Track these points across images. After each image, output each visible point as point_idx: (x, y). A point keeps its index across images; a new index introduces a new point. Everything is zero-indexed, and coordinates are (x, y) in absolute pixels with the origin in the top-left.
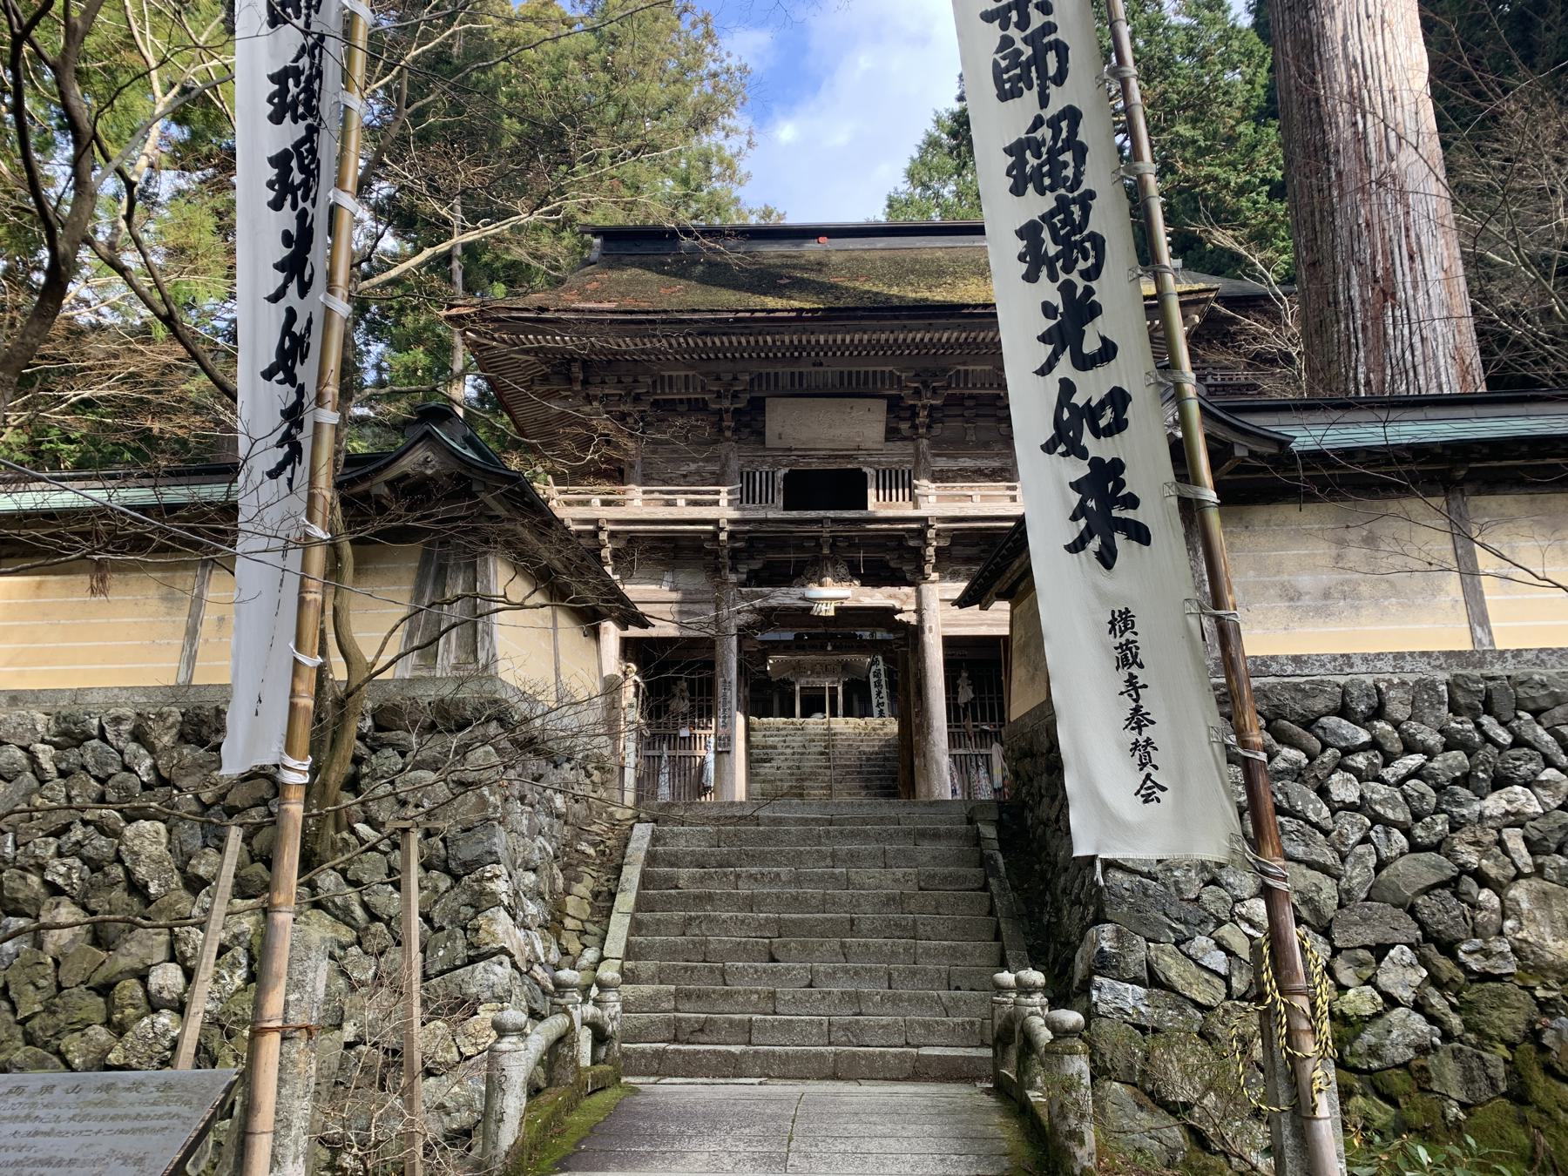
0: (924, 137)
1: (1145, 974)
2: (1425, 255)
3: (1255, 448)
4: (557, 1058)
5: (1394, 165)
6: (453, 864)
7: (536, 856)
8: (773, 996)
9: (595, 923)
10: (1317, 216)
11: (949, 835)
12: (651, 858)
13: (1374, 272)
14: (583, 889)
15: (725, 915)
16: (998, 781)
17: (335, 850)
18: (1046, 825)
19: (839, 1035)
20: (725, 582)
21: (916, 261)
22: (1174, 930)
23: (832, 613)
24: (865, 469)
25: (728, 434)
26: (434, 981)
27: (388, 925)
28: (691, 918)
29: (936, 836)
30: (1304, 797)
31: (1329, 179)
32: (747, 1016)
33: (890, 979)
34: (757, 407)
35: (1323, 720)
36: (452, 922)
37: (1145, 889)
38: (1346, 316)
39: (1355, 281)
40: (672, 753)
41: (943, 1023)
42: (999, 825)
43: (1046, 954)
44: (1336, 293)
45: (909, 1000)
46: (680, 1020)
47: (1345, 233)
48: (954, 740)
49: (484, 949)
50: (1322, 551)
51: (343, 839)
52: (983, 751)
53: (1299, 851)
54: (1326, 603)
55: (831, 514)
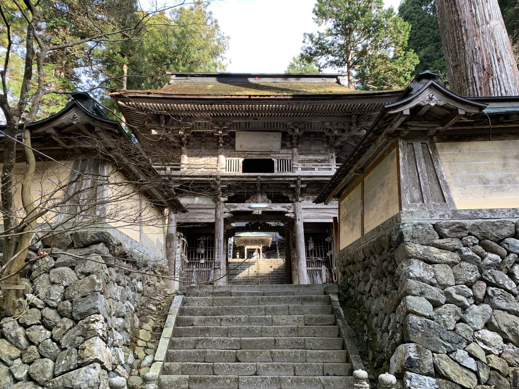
0: (289, 64)
1: (433, 371)
2: (504, 59)
3: (468, 111)
5: (488, 25)
6: (74, 315)
7: (124, 310)
9: (152, 343)
10: (457, 47)
11: (317, 300)
12: (182, 311)
13: (483, 67)
14: (148, 326)
15: (215, 339)
16: (324, 280)
17: (15, 307)
18: (362, 294)
21: (292, 85)
22: (446, 346)
24: (273, 159)
25: (221, 145)
26: (57, 378)
27: (38, 347)
28: (198, 340)
29: (311, 300)
30: (502, 277)
31: (462, 32)
34: (233, 135)
35: (507, 240)
36: (71, 345)
37: (429, 325)
38: (472, 84)
39: (475, 70)
40: (197, 269)
42: (339, 295)
43: (367, 356)
44: (467, 76)
45: (305, 381)
50: (497, 162)
51: (19, 302)
52: (319, 268)
53: (503, 304)
54: (501, 185)
55: (261, 174)
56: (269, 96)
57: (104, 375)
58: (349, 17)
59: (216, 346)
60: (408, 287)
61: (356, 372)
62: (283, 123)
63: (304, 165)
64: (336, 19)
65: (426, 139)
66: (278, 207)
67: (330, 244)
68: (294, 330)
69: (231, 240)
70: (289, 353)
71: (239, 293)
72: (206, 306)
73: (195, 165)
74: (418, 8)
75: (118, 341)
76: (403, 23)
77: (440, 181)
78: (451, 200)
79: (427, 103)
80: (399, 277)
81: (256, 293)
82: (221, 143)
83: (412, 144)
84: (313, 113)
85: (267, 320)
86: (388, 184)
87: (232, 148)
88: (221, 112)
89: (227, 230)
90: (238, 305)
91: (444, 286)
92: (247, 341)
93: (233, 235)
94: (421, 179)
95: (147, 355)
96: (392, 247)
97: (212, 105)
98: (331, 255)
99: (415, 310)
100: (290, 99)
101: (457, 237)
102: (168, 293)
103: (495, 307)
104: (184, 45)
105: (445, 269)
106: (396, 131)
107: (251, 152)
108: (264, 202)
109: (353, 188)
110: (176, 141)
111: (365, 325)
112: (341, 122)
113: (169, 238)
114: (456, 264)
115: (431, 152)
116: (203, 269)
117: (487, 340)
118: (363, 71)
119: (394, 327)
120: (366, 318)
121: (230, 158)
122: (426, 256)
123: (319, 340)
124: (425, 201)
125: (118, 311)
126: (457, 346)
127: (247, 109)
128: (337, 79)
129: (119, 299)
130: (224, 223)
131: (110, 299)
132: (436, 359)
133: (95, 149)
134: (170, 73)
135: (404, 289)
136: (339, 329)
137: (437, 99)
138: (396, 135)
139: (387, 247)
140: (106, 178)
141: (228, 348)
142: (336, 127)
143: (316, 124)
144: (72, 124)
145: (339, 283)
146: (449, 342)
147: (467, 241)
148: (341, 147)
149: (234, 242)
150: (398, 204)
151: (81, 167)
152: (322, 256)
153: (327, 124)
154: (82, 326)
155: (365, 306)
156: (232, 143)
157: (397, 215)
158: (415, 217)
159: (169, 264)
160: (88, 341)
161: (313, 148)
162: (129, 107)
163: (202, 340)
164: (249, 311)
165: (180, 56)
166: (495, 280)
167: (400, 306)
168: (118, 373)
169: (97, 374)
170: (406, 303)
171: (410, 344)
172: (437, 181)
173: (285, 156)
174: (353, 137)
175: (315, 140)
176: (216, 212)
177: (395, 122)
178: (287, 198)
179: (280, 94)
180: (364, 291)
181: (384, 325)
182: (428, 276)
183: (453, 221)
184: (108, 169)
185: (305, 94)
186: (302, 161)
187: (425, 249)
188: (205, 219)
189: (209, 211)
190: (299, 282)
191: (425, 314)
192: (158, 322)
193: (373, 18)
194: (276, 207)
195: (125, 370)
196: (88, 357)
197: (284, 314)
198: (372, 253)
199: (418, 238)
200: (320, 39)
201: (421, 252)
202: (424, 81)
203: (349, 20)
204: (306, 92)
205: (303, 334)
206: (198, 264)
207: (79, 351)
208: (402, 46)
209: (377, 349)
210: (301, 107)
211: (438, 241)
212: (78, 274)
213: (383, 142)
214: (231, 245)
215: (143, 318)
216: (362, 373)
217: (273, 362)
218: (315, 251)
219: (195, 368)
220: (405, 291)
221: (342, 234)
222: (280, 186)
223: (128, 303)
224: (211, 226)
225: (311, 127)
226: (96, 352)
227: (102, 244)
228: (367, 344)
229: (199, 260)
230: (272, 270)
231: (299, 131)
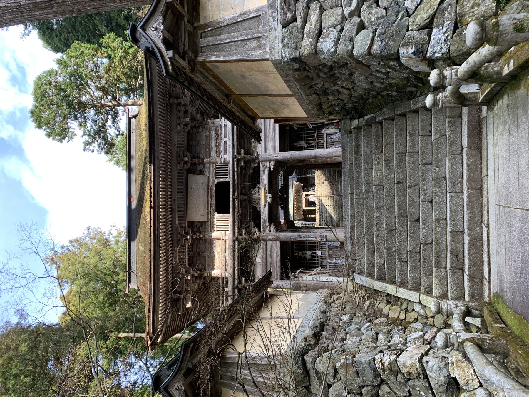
0: (115, 165)
1: (426, 31)
4: (491, 349)
6: (376, 383)
7: (370, 333)
8: (437, 220)
9: (402, 304)
11: (357, 141)
12: (370, 275)
18: (351, 96)
19: (457, 188)
20: (258, 237)
21: (139, 164)
22: (402, 18)
23: (270, 195)
24: (216, 183)
25: (202, 236)
28: (399, 259)
29: (357, 147)
32: (449, 234)
33: (427, 164)
34: (191, 224)
37: (381, 34)
41: (450, 136)
42: (352, 119)
43: (411, 92)
45: (437, 154)
46: (452, 267)
48: (321, 147)
49: (420, 371)
52: (325, 136)
55: (231, 195)
56: (151, 187)
57: (434, 353)
58: (67, 105)
59: (404, 241)
60: (345, 54)
61: (428, 106)
62: (178, 173)
63: (222, 151)
64: (68, 118)
65: (197, 33)
66: (264, 178)
67: (300, 125)
68: (387, 164)
69: (298, 223)
70: (410, 169)
71: (351, 218)
72: (365, 251)
73: (222, 263)
74: (56, 32)
75: (401, 339)
76: (72, 49)
77: (239, 20)
78: (258, 10)
79: (161, 33)
80: (335, 62)
81: (351, 201)
82: (199, 236)
83: (202, 47)
84: (168, 142)
85: (378, 191)
86: (242, 71)
87: (205, 225)
88: (167, 236)
89: (288, 228)
90: (363, 219)
91: (344, 18)
92: (399, 210)
93: (293, 222)
94: (237, 39)
95: (413, 310)
96: (305, 68)
97: (160, 247)
98: (312, 124)
99: (367, 47)
100: (154, 166)
101: (295, 4)
102: (352, 289)
104: (97, 274)
105: (327, 17)
107: (209, 205)
108: (259, 192)
109: (246, 105)
110: (198, 282)
111: (382, 93)
112: (177, 114)
113: (297, 288)
114: (321, 6)
115: (210, 29)
116: (327, 254)
118: (123, 90)
119: (384, 66)
120: (374, 93)
121: (215, 226)
122: (314, 35)
123: (397, 139)
124: (260, 35)
125: (371, 340)
126: (401, 6)
127: (164, 210)
128: (132, 118)
129: (360, 338)
130: (280, 232)
131: (360, 347)
132: (415, 27)
133: (211, 368)
134: (127, 289)
135: (347, 57)
136: (386, 119)
137: (157, 23)
138: (193, 63)
139: (306, 73)
140: (240, 355)
141: (406, 229)
142: (182, 119)
143: (179, 139)
144: (185, 390)
145: (340, 118)
146: (398, 15)
148: (202, 114)
149: (299, 220)
150: (263, 62)
151: (228, 380)
152: (312, 133)
153: (179, 128)
154: (387, 376)
155: (363, 93)
156: (199, 225)
157: (273, 63)
158: (275, 46)
159: (323, 288)
160: (401, 369)
161: (204, 142)
162: (163, 331)
163: (398, 255)
164: (369, 209)
165: (109, 279)
167: (363, 62)
168: (432, 338)
169: (434, 359)
170: (360, 56)
171: (400, 52)
172: (239, 23)
173: (212, 171)
174: (192, 101)
175: (195, 140)
176: (270, 240)
177: (180, 65)
178: (254, 168)
179: (149, 177)
180: (349, 94)
181: (382, 76)
182: (333, 34)
183: (279, 9)
184: (229, 353)
185: (148, 151)
187: (307, 36)
188: (277, 252)
189: (269, 248)
190: (339, 156)
191: (371, 38)
192: (381, 299)
193: (68, 80)
194: (264, 180)
195: (429, 331)
196: (417, 369)
197: (372, 173)
198: (311, 87)
199: (297, 43)
200: (89, 135)
201: (310, 40)
202: (138, 35)
203: (70, 105)
204: (146, 150)
205: (391, 155)
206: (322, 257)
207: (411, 378)
208: (96, 51)
209: (405, 82)
210: (161, 155)
211: (299, 23)
212: (336, 380)
213: (200, 76)
214: (302, 224)
215: (378, 314)
216: (429, 100)
217: (419, 185)
218: (307, 140)
219: (426, 262)
220: (349, 56)
221: (292, 115)
222: (243, 176)
223: (363, 330)
224: (285, 246)
225: (183, 144)
226: (412, 361)
227: (305, 357)
228: (400, 92)
229: (318, 257)
230: (326, 182)
231: (186, 156)
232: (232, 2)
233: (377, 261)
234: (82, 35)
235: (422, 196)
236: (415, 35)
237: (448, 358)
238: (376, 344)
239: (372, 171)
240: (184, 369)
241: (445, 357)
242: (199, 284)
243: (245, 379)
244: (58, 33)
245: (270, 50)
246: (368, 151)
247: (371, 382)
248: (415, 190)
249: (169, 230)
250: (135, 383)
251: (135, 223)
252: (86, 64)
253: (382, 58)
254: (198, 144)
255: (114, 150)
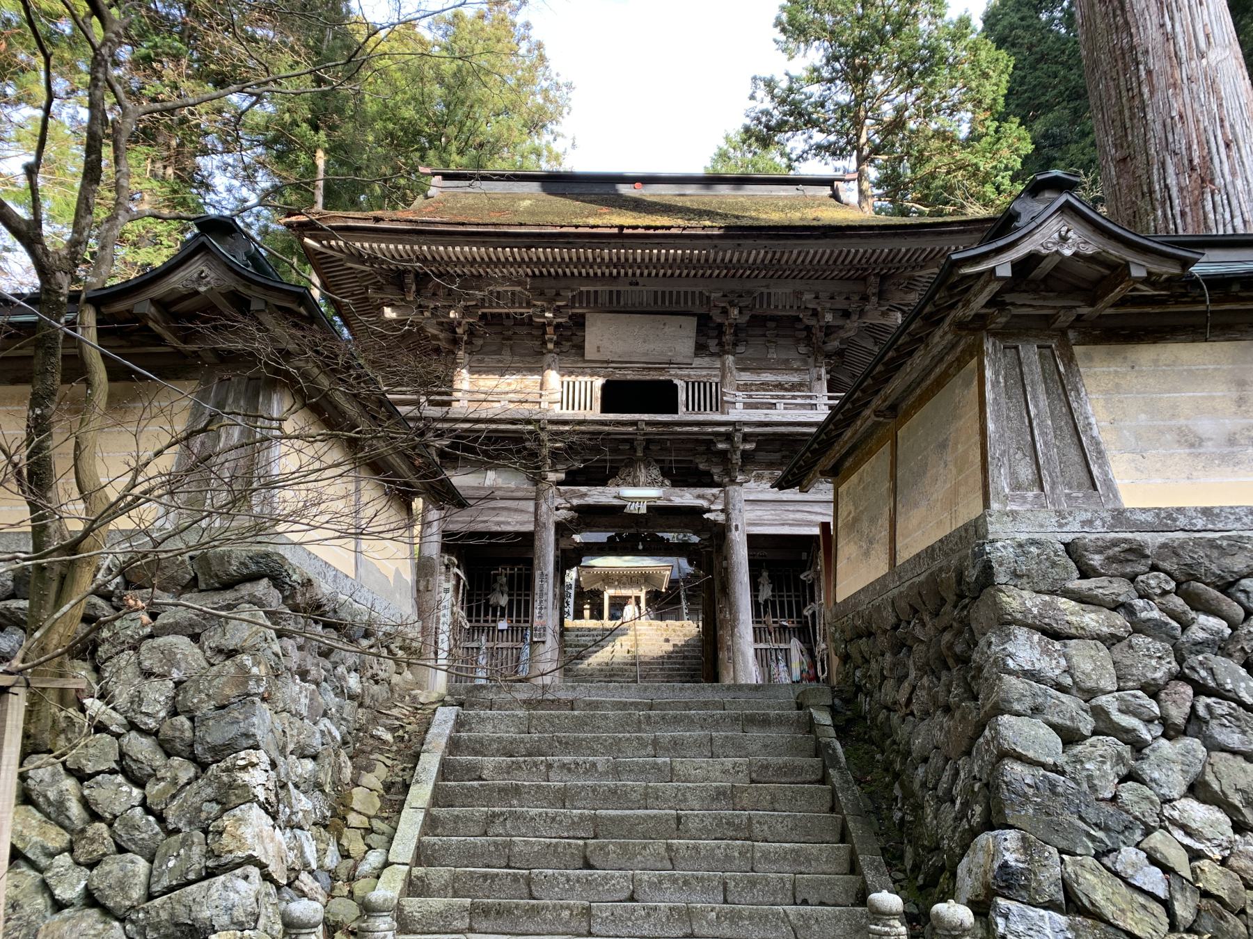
0: (716, 151)
2: (1241, 144)
5: (1204, 61)
6: (199, 750)
7: (317, 741)
9: (384, 819)
11: (780, 721)
12: (454, 745)
13: (1191, 161)
14: (373, 780)
15: (534, 811)
16: (796, 674)
18: (889, 710)
21: (722, 203)
22: (1093, 839)
23: (644, 511)
24: (676, 381)
25: (550, 346)
26: (157, 902)
27: (110, 825)
28: (494, 815)
29: (765, 722)
30: (1232, 674)
31: (1138, 78)
33: (725, 890)
34: (579, 323)
35: (1243, 581)
36: (190, 823)
37: (1053, 786)
38: (1163, 204)
39: (1171, 170)
40: (491, 644)
42: (833, 710)
43: (901, 858)
44: (1150, 184)
45: (751, 918)
47: (1158, 127)
48: (758, 635)
52: (783, 646)
55: (646, 417)
56: (669, 228)
57: (268, 894)
58: (862, 39)
59: (535, 829)
60: (1002, 694)
62: (701, 293)
63: (750, 397)
65: (1051, 337)
66: (686, 497)
67: (812, 586)
68: (724, 793)
69: (571, 575)
71: (592, 702)
73: (484, 392)
74: (1031, 17)
75: (301, 814)
76: (994, 54)
77: (1084, 439)
78: (1109, 484)
79: (1055, 249)
80: (980, 669)
81: (632, 704)
83: (1016, 348)
84: (775, 270)
85: (659, 770)
86: (956, 444)
87: (577, 354)
88: (552, 266)
89: (563, 551)
90: (591, 732)
91: (1090, 694)
93: (578, 563)
94: (1036, 432)
95: (370, 848)
97: (528, 248)
98: (813, 614)
99: (1019, 750)
101: (1123, 575)
102: (422, 700)
103: (1213, 746)
104: (463, 103)
105: (1093, 653)
106: (978, 317)
107: (623, 364)
108: (652, 484)
109: (871, 453)
110: (442, 336)
111: (897, 785)
112: (840, 293)
113: (423, 568)
115: (1062, 369)
116: (505, 645)
117: (1194, 826)
120: (898, 767)
121: (573, 378)
124: (1047, 487)
126: (1121, 837)
127: (615, 260)
129: (305, 714)
131: (284, 714)
132: (1069, 870)
133: (251, 354)
134: (428, 171)
135: (994, 698)
136: (833, 793)
137: (1079, 240)
138: (979, 324)
139: (951, 598)
141: (566, 834)
142: (828, 305)
143: (781, 297)
144: (197, 293)
146: (1100, 829)
147: (1148, 585)
148: (840, 353)
149: (577, 581)
150: (979, 494)
151: (216, 395)
152: (791, 616)
153: (808, 296)
154: (217, 777)
156: (576, 340)
158: (1021, 524)
160: (232, 812)
161: (773, 355)
162: (331, 252)
163: (502, 814)
164: (615, 747)
165: (451, 130)
166: (1215, 680)
167: (981, 740)
169: (252, 894)
170: (998, 733)
172: (1075, 439)
173: (704, 373)
174: (871, 329)
175: (777, 336)
176: (537, 507)
179: (693, 223)
180: (895, 703)
182: (1052, 667)
183: (1113, 535)
184: (281, 401)
185: (756, 223)
186: (746, 387)
187: (1045, 603)
188: (509, 523)
190: (735, 678)
191: (1042, 759)
192: (396, 770)
193: (921, 41)
194: (682, 497)
196: (230, 852)
197: (701, 755)
200: (790, 90)
201: (1035, 610)
202: (1048, 195)
203: (862, 46)
204: (758, 219)
205: (745, 802)
206: (492, 632)
207: (210, 836)
208: (990, 108)
209: (926, 843)
210: (745, 254)
211: (1076, 584)
212: (209, 653)
213: (944, 342)
215: (362, 761)
216: (889, 900)
217: (673, 869)
218: (773, 603)
219: (485, 880)
220: (996, 703)
221: (842, 565)
223: (325, 723)
224: (526, 540)
225: (769, 304)
226: (249, 841)
227: (265, 581)
228: (900, 829)
229: (494, 621)
230: (669, 647)
231: (740, 312)
232: (1128, 423)
233: (489, 763)
234: (1025, 77)
235: (646, 877)
236: (1050, 872)
237: (255, 928)
238: (292, 753)
239: (705, 756)
240: (250, 293)
241: (256, 921)
242: (439, 340)
243: (219, 436)
244: (1029, 22)
245: (1012, 512)
246: (755, 748)
247: (202, 739)
248: (663, 858)
249: (567, 270)
250: (208, 187)
251: (583, 191)
252: (960, 85)
253: (991, 785)
254: (769, 341)
255: (755, 145)
